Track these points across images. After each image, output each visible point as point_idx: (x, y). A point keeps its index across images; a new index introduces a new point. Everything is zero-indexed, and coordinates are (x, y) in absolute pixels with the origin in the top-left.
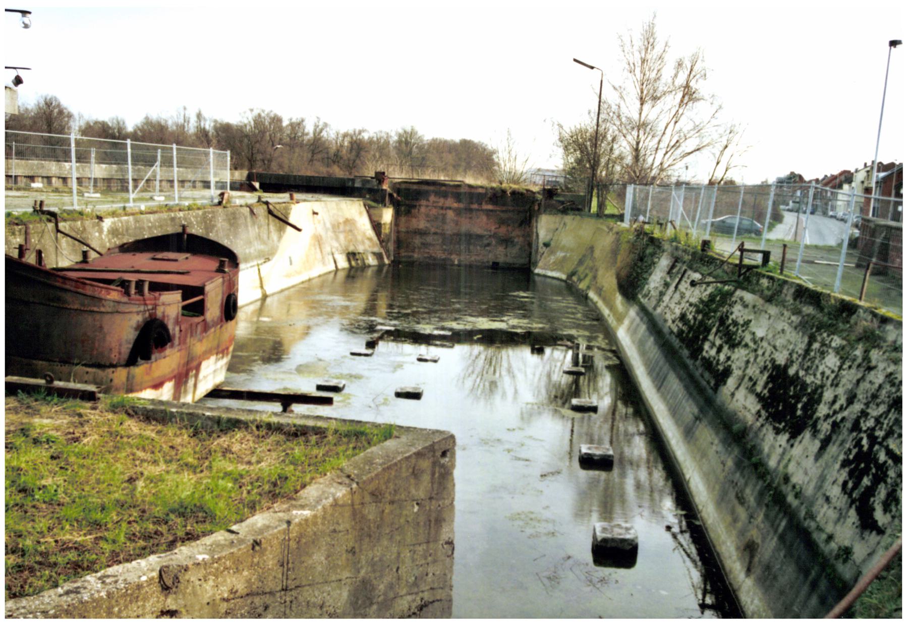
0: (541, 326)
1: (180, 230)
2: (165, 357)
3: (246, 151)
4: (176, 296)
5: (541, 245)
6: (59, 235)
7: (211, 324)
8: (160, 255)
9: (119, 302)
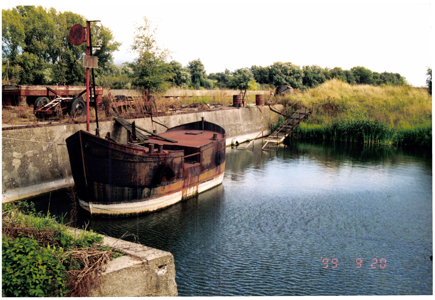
0: (97, 197)
1: (201, 120)
2: (173, 183)
3: (81, 73)
4: (182, 153)
5: (216, 133)
6: (153, 122)
7: (205, 167)
8: (189, 132)
9: (143, 157)
